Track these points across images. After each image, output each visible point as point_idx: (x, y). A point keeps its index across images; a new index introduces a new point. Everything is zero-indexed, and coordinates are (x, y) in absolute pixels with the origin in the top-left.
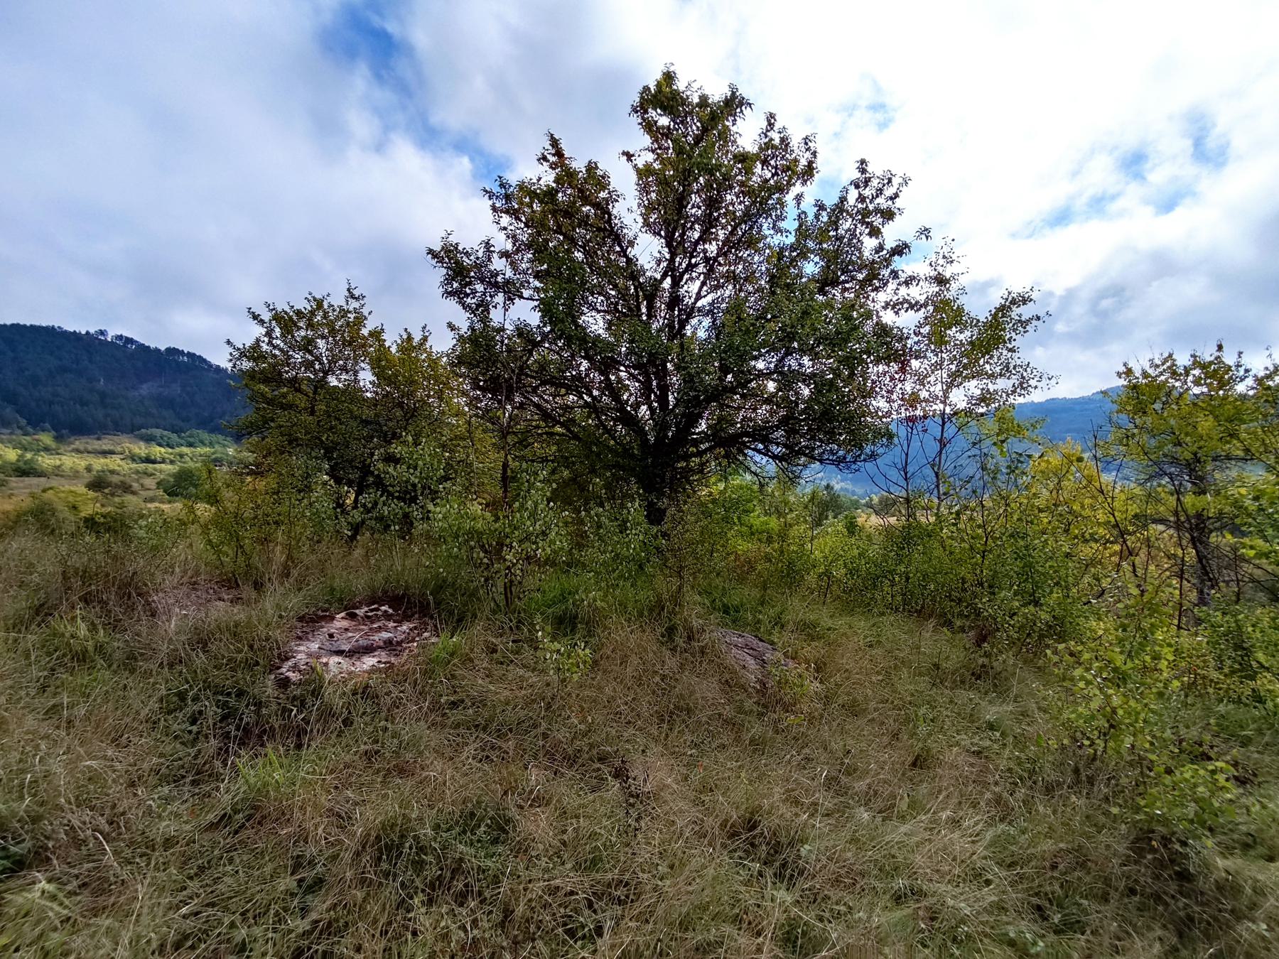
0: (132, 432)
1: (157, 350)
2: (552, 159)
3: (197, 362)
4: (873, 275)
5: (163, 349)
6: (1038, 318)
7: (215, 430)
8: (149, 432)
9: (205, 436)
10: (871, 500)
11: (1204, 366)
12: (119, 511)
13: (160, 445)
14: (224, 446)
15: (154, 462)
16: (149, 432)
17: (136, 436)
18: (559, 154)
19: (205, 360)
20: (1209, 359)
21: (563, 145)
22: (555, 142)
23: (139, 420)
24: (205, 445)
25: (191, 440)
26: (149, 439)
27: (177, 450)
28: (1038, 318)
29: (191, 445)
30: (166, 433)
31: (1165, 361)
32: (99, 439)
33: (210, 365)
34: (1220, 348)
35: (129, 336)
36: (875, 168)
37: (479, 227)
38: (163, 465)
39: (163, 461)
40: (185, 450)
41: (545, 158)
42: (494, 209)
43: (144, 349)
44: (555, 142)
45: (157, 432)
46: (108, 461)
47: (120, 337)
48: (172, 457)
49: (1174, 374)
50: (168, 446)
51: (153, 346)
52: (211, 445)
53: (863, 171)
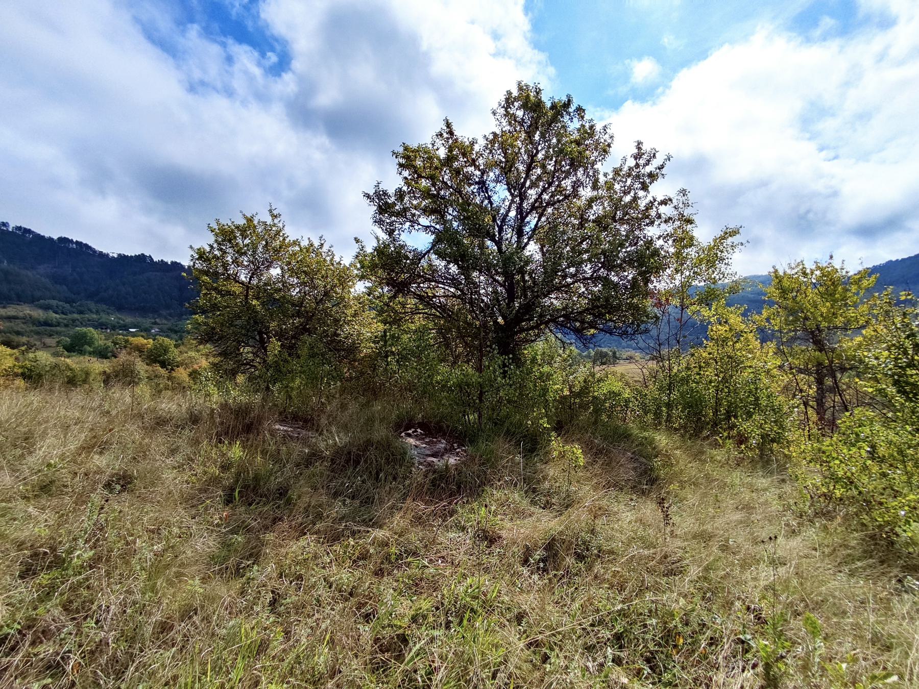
0: (33, 302)
1: (51, 239)
2: (445, 135)
3: (176, 266)
4: (647, 217)
5: (55, 238)
6: (742, 244)
7: (102, 301)
8: (47, 302)
9: (92, 305)
10: (589, 353)
11: (821, 269)
12: (33, 364)
13: (56, 313)
14: (108, 314)
15: (51, 325)
16: (47, 302)
17: (36, 306)
18: (451, 133)
19: (90, 247)
20: (825, 265)
21: (454, 128)
22: (448, 125)
23: (38, 294)
24: (92, 312)
25: (82, 309)
26: (46, 308)
27: (70, 316)
28: (742, 244)
29: (81, 312)
30: (61, 303)
31: (798, 265)
32: (4, 307)
33: (94, 251)
34: (831, 257)
35: (28, 227)
36: (646, 147)
37: (393, 181)
38: (58, 328)
39: (58, 324)
40: (76, 316)
41: (441, 135)
42: (401, 165)
43: (40, 238)
44: (448, 125)
45: (54, 303)
46: (12, 324)
47: (19, 228)
48: (65, 321)
49: (805, 274)
50: (63, 313)
51: (47, 235)
52: (97, 312)
53: (639, 148)
